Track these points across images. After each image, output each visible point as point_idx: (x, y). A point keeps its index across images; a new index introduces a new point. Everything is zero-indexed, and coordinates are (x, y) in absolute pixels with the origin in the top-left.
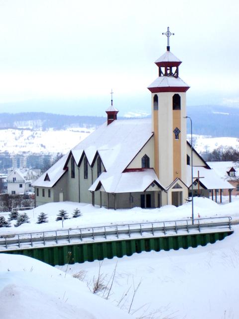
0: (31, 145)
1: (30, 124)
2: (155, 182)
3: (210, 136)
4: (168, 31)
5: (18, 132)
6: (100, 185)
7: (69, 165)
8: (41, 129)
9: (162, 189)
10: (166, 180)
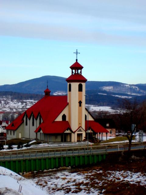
3: (107, 88)
4: (77, 52)
8: (10, 100)
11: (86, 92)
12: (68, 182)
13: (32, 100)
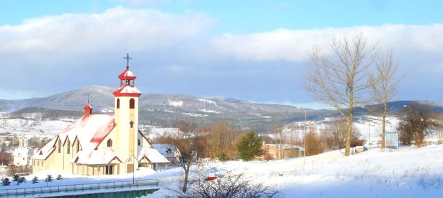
1: (34, 115)
2: (116, 157)
5: (24, 121)
7: (57, 145)
10: (124, 156)
11: (139, 108)
12: (324, 176)
13: (70, 118)
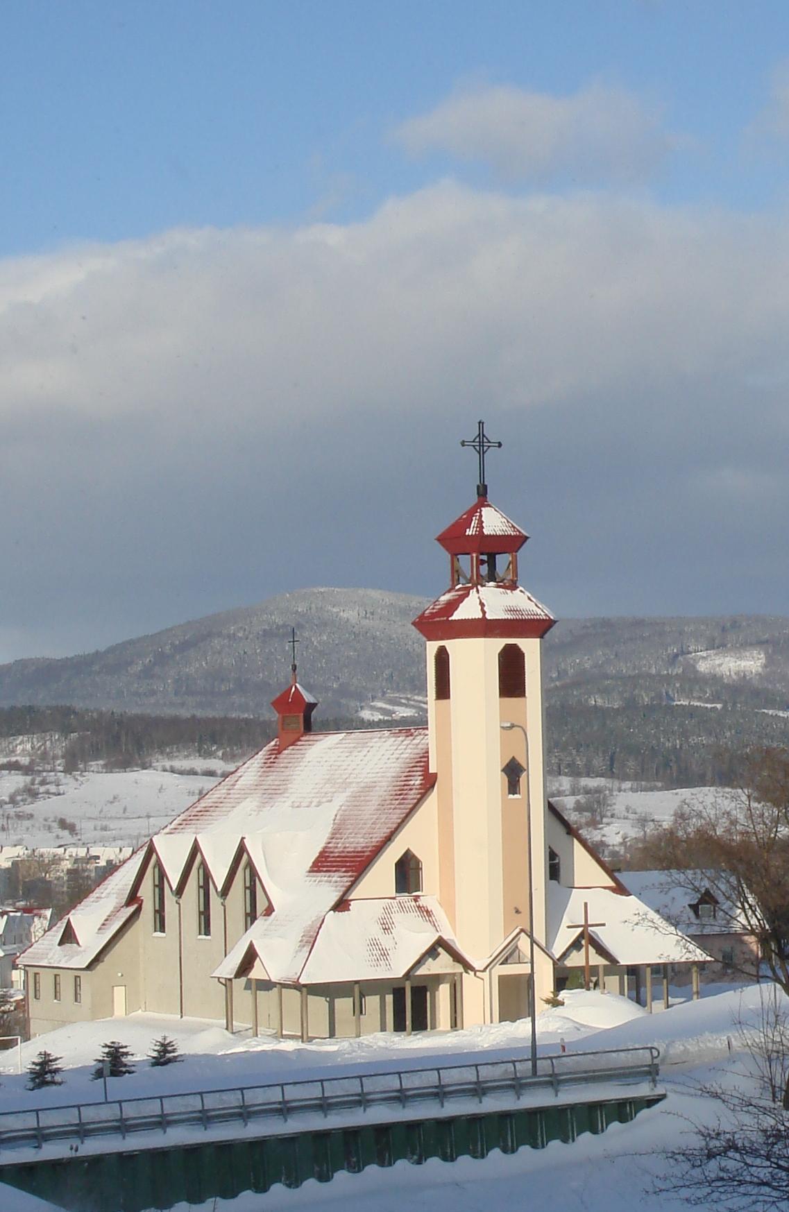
0: (27, 823)
2: (441, 943)
3: (659, 784)
4: (481, 435)
6: (250, 957)
8: (60, 764)
9: (468, 967)
10: (480, 938)
11: (546, 693)
13: (208, 755)
